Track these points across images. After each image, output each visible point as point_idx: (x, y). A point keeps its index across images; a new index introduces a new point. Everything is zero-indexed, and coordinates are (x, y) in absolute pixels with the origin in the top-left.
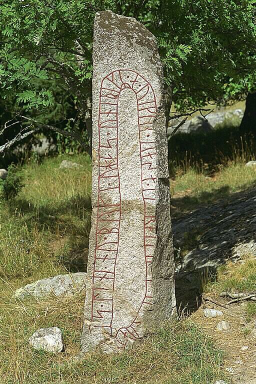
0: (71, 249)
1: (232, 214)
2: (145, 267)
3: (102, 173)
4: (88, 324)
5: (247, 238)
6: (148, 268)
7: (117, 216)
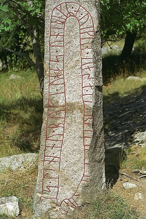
0: (20, 134)
1: (128, 111)
2: (84, 153)
3: (52, 81)
4: (40, 196)
5: (143, 128)
6: (86, 154)
7: (63, 115)
